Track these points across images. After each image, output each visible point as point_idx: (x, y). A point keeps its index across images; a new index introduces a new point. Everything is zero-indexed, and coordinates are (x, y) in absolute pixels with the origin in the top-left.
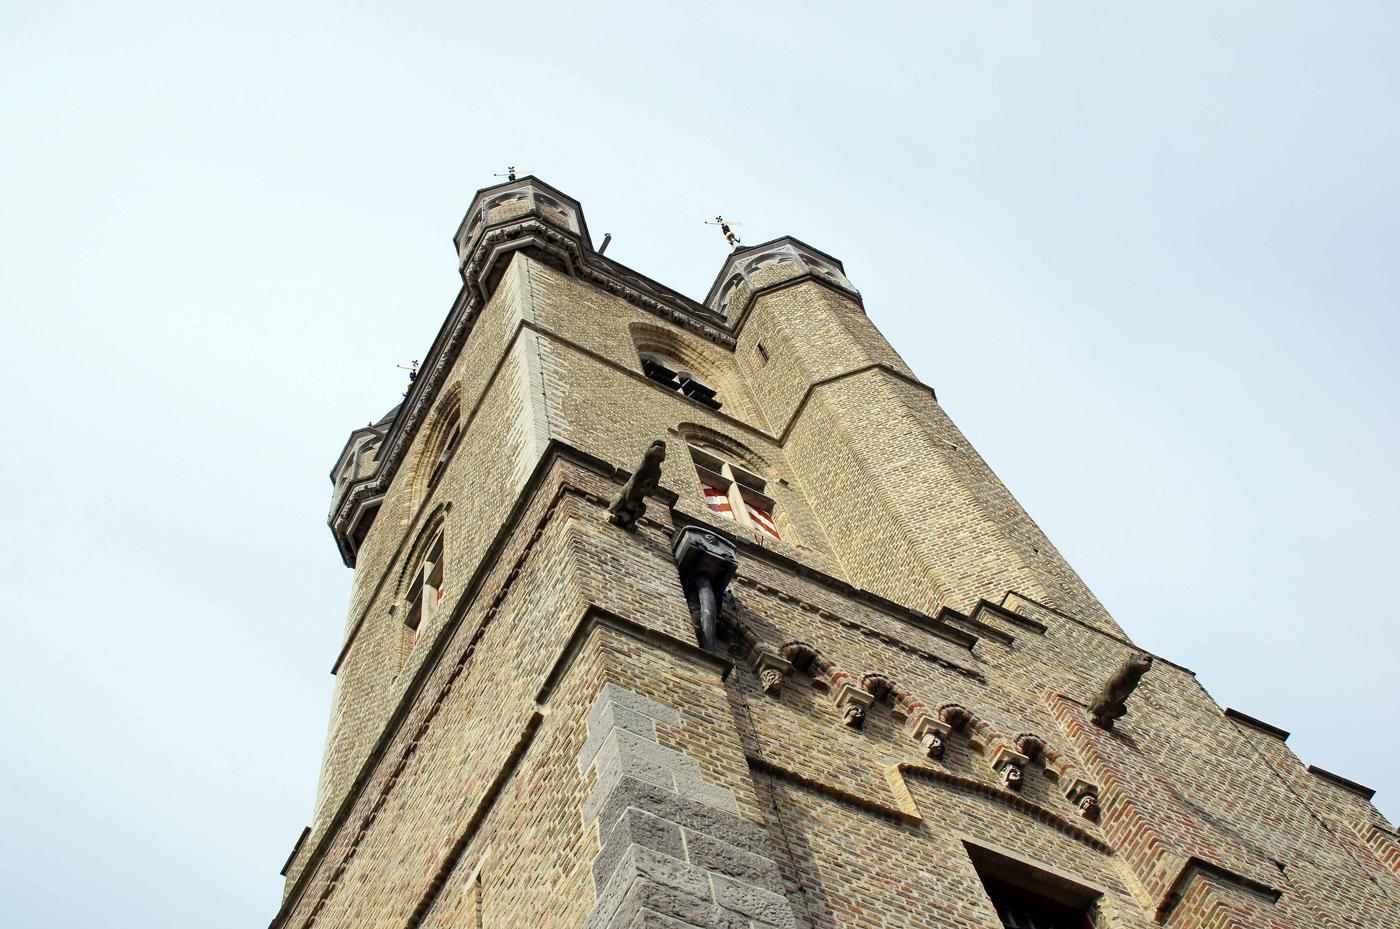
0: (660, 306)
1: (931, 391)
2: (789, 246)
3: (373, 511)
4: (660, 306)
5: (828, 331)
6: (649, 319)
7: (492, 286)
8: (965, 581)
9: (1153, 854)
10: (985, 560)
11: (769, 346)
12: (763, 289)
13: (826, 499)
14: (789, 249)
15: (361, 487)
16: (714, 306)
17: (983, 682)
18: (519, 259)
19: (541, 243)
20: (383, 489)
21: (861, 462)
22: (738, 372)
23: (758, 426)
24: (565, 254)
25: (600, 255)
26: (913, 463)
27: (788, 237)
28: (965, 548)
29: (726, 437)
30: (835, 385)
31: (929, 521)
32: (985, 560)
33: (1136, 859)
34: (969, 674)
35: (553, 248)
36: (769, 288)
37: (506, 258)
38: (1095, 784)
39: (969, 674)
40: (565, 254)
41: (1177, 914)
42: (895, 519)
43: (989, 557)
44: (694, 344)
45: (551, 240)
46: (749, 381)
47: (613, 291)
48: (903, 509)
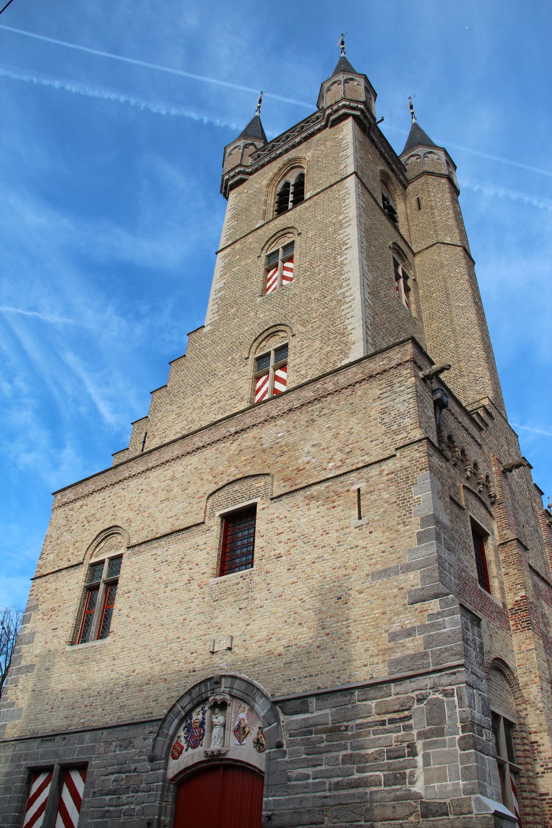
0: (389, 160)
1: (474, 263)
2: (443, 152)
3: (242, 181)
4: (389, 160)
5: (448, 214)
6: (387, 170)
7: (335, 123)
8: (470, 374)
9: (505, 527)
10: (479, 369)
11: (423, 203)
12: (428, 172)
13: (427, 297)
14: (442, 154)
15: (242, 169)
16: (403, 160)
17: (481, 448)
18: (350, 119)
19: (362, 117)
20: (251, 174)
21: (448, 295)
22: (405, 205)
23: (408, 241)
24: (368, 125)
25: (376, 124)
26: (465, 306)
27: (444, 149)
28: (473, 359)
29: (403, 251)
30: (446, 248)
31: (465, 339)
32: (479, 369)
33: (499, 525)
34: (479, 445)
35: (365, 121)
36: (431, 173)
37: (345, 117)
38: (497, 495)
39: (479, 445)
40: (368, 125)
41: (504, 547)
42: (454, 331)
43: (480, 369)
44: (395, 184)
45: (366, 117)
46: (409, 211)
47: (376, 147)
48: (457, 327)
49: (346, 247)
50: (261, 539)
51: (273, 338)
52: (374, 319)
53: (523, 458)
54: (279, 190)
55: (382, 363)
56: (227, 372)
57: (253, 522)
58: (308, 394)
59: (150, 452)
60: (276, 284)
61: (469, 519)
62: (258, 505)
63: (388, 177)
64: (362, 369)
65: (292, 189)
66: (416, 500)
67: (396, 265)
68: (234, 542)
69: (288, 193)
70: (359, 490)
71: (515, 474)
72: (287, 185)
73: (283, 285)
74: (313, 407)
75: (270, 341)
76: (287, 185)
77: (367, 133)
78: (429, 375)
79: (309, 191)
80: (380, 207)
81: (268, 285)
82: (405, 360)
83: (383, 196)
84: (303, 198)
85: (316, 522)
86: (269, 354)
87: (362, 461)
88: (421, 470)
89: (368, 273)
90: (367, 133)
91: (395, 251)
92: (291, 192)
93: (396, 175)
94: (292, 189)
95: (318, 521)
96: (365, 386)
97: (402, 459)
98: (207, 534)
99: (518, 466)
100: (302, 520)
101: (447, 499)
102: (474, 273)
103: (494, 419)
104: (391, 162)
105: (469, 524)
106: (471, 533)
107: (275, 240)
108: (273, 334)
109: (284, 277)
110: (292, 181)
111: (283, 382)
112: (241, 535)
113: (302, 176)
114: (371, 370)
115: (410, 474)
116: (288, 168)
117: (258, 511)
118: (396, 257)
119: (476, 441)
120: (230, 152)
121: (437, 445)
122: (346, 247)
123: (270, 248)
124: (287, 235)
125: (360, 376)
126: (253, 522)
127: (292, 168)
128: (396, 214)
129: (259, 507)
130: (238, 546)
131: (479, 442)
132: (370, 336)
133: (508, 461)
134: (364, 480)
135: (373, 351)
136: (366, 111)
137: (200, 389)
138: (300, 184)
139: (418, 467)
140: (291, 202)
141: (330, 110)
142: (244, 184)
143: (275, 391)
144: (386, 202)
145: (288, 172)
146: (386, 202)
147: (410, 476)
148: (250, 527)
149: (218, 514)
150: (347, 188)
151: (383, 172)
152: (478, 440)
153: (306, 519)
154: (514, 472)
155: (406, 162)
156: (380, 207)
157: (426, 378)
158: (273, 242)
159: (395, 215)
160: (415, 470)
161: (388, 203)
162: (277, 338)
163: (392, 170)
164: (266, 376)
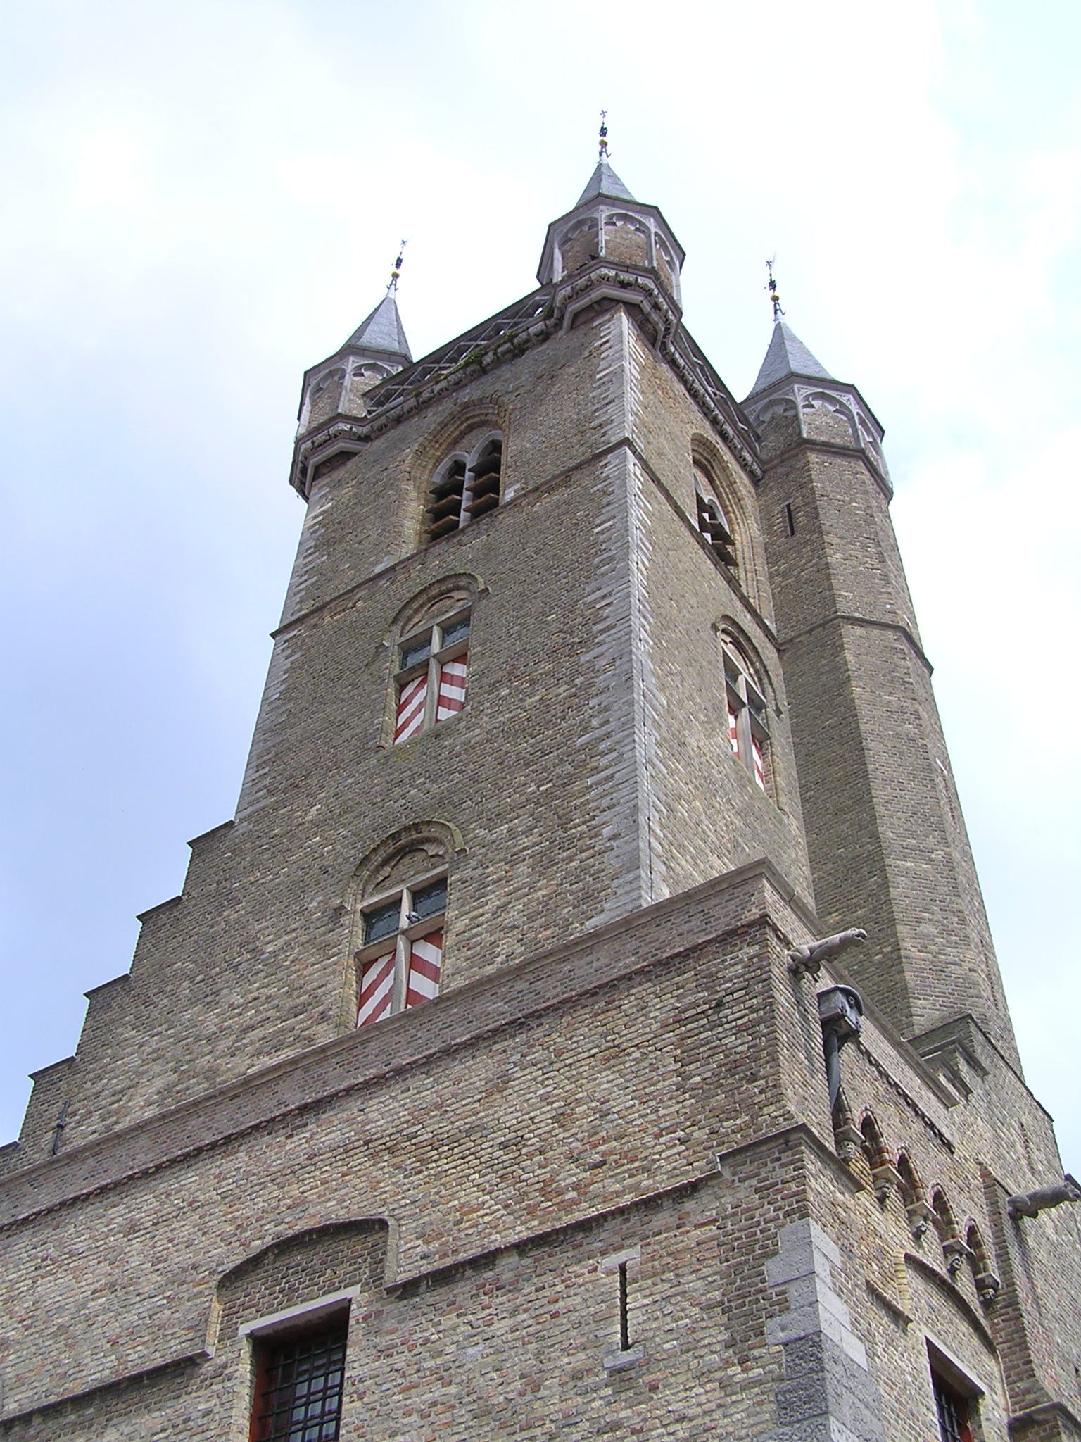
1: (931, 670)
3: (345, 456)
20: (366, 439)
45: (656, 306)
49: (600, 626)
50: (358, 1404)
51: (408, 857)
52: (671, 809)
53: (1069, 1178)
54: (437, 479)
55: (686, 927)
56: (288, 944)
57: (339, 1356)
58: (497, 1009)
59: (73, 1157)
60: (420, 717)
61: (924, 1349)
62: (354, 1306)
63: (714, 452)
64: (635, 943)
65: (468, 479)
66: (775, 1299)
67: (732, 673)
68: (288, 1406)
69: (458, 489)
70: (623, 1269)
71: (1049, 1222)
72: (459, 468)
73: (437, 721)
74: (506, 1043)
75: (400, 866)
76: (459, 468)
77: (659, 344)
78: (810, 958)
79: (511, 484)
80: (691, 528)
81: (402, 719)
82: (744, 922)
83: (700, 500)
84: (495, 503)
85: (505, 1356)
86: (396, 903)
87: (630, 1189)
88: (787, 1215)
89: (658, 694)
90: (659, 344)
91: (728, 639)
92: (464, 506)
93: (732, 449)
94: (468, 479)
95: (513, 1352)
96: (643, 990)
97: (737, 1184)
98: (214, 1387)
99: (1055, 1198)
100: (470, 1351)
101: (862, 1294)
102: (932, 695)
103: (987, 1073)
104: (720, 417)
105: (925, 1361)
106: (930, 1389)
107: (422, 606)
108: (442, 595)
109: (442, 701)
110: (471, 460)
111: (433, 973)
112: (302, 1417)
113: (496, 447)
114: (657, 944)
115: (758, 1223)
116: (462, 427)
117: (352, 1322)
118: (730, 650)
119: (941, 1135)
120: (318, 384)
121: (831, 1146)
122: (600, 626)
123: (408, 628)
124: (452, 594)
125: (631, 963)
126: (339, 1356)
127: (471, 428)
128: (733, 544)
129: (356, 1312)
130: (298, 1422)
131: (947, 1136)
132: (658, 856)
133: (1021, 1187)
134: (636, 1239)
135: (668, 896)
136: (656, 292)
137: (215, 988)
138: (491, 464)
139: (780, 1209)
140: (467, 490)
141: (569, 288)
142: (350, 465)
143: (412, 996)
144: (706, 516)
145: (463, 435)
146: (706, 516)
147: (758, 1230)
148: (332, 1368)
149: (244, 1329)
150: (608, 477)
151: (699, 441)
152: (944, 1130)
153: (480, 1347)
154: (1042, 1215)
155: (758, 417)
156: (691, 528)
157: (802, 968)
158: (416, 611)
159: (730, 548)
160: (772, 1214)
161: (713, 517)
162: (419, 857)
163: (724, 436)
164: (390, 957)
